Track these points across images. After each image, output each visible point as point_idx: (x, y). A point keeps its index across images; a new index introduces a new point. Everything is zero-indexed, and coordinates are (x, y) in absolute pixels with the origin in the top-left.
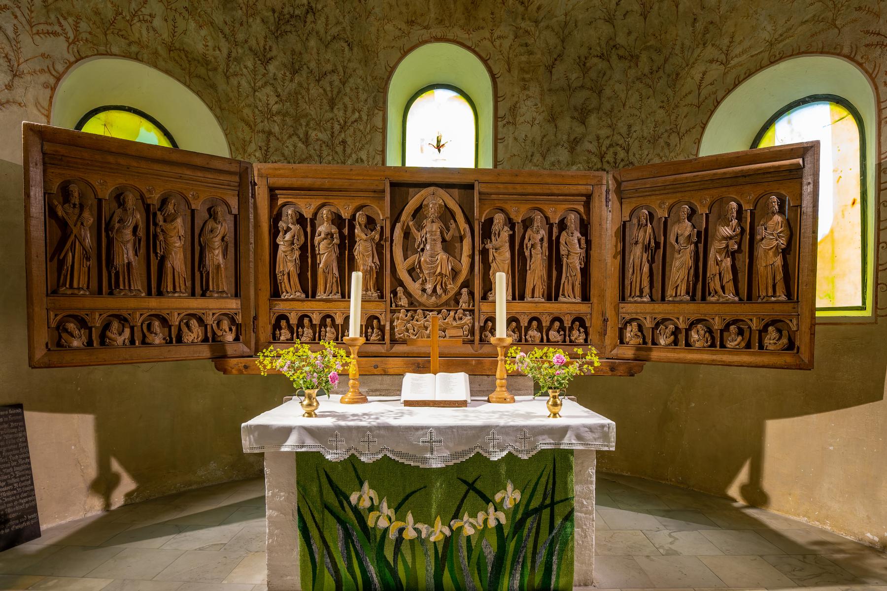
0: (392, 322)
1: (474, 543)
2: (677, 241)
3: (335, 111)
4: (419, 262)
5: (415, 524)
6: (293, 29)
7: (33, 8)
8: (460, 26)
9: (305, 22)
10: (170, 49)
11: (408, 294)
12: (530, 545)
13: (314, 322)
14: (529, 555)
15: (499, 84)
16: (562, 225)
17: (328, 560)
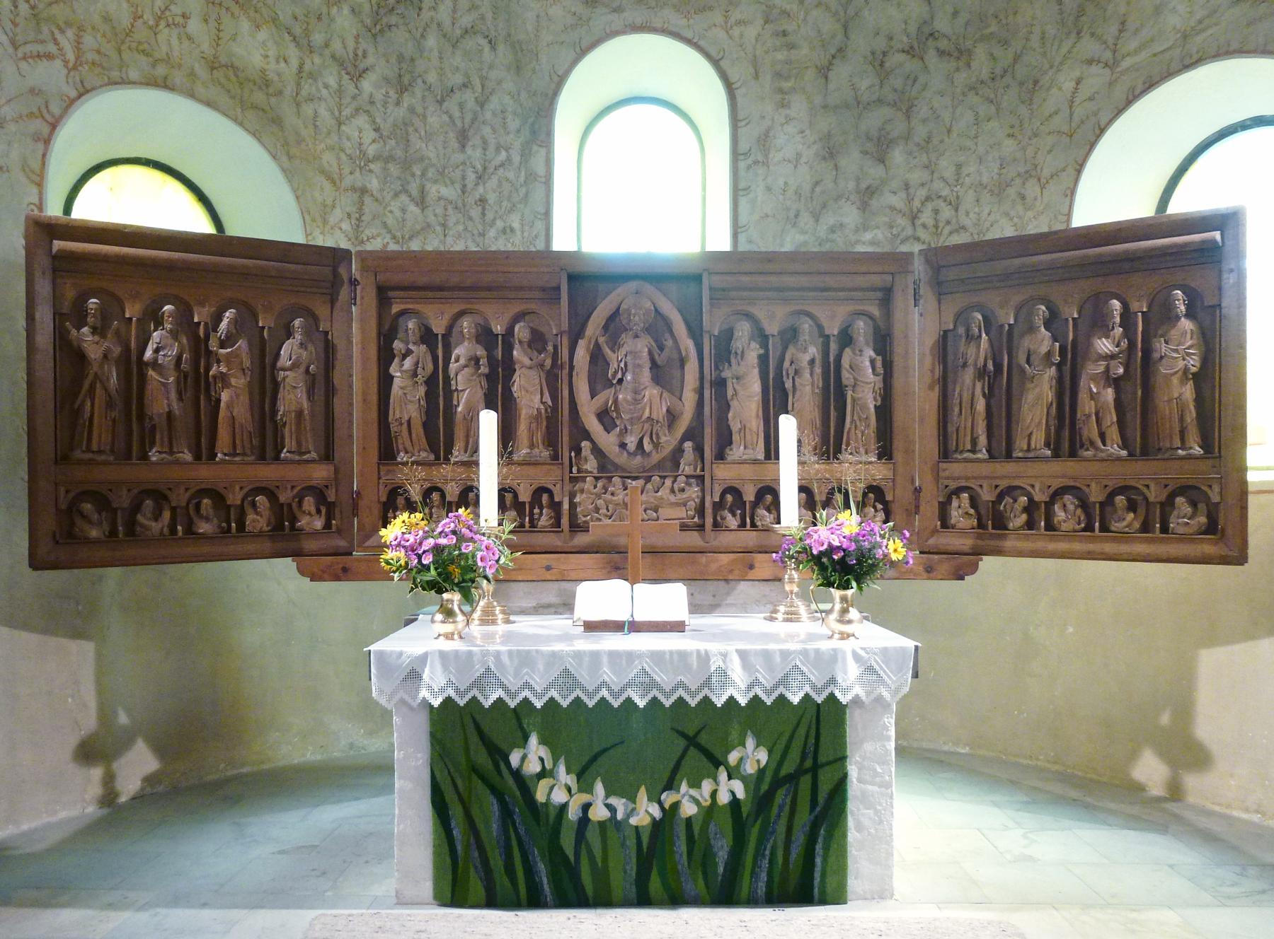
0: (572, 496)
1: (696, 829)
2: (1028, 362)
3: (469, 151)
4: (616, 401)
5: (607, 797)
6: (401, 21)
7: (18, 20)
8: (674, 6)
9: (420, 9)
10: (213, 65)
11: (597, 451)
12: (781, 828)
13: (522, 499)
14: (780, 844)
15: (739, 99)
16: (846, 339)
17: (476, 854)
